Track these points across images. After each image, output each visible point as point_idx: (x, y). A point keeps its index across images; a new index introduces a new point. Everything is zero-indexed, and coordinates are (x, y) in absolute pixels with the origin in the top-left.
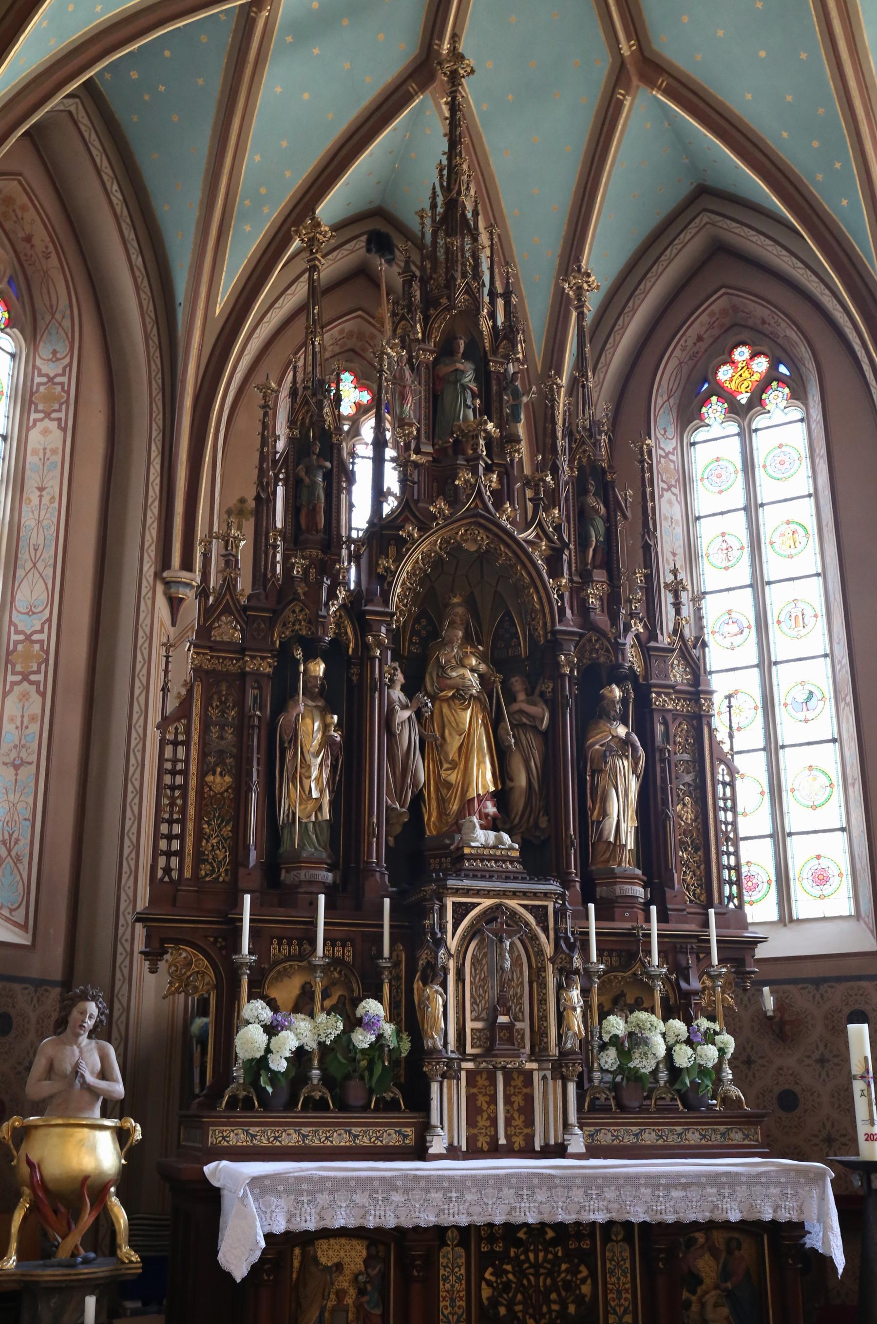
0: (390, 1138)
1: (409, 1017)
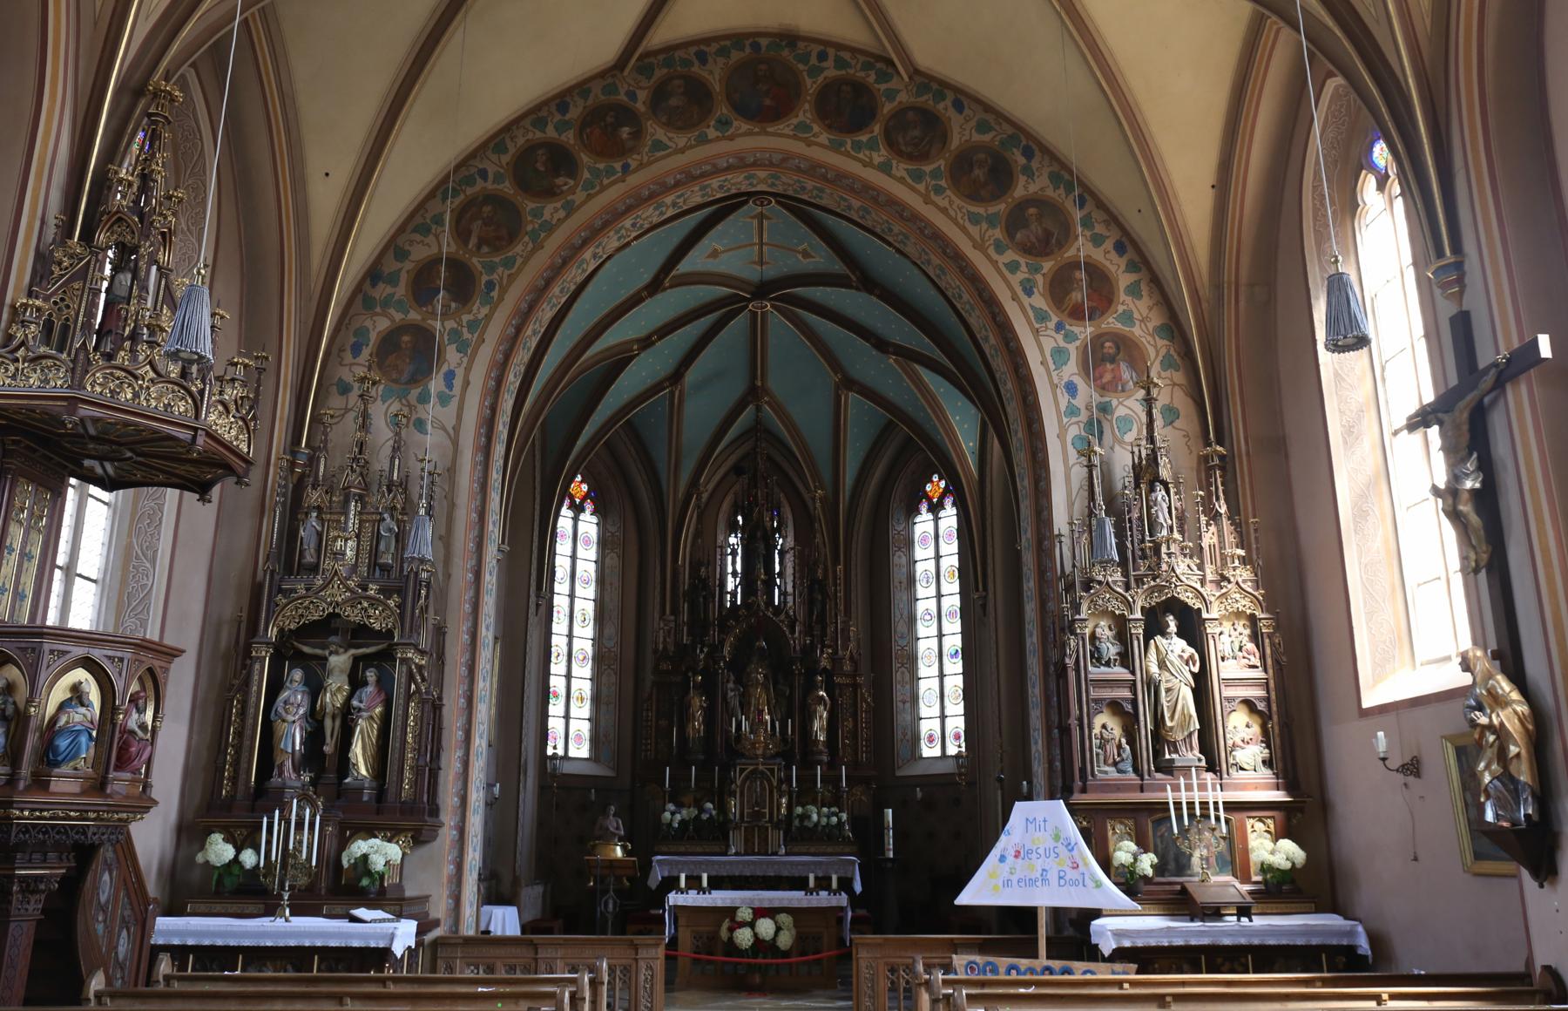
0: (717, 849)
1: (722, 807)
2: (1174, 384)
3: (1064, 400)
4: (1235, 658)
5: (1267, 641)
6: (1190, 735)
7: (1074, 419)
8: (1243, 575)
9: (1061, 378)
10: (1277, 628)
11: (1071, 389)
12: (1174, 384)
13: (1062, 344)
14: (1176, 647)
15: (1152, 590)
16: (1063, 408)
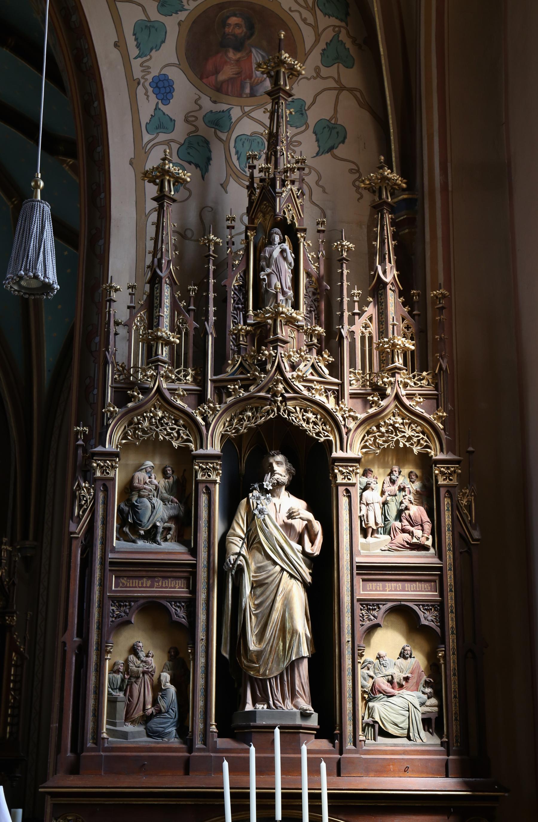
2: (342, 88)
3: (147, 106)
4: (387, 531)
5: (446, 502)
6: (292, 666)
7: (163, 137)
8: (408, 386)
9: (146, 70)
10: (465, 480)
11: (163, 88)
12: (342, 88)
13: (155, 15)
14: (281, 508)
15: (242, 405)
16: (145, 118)
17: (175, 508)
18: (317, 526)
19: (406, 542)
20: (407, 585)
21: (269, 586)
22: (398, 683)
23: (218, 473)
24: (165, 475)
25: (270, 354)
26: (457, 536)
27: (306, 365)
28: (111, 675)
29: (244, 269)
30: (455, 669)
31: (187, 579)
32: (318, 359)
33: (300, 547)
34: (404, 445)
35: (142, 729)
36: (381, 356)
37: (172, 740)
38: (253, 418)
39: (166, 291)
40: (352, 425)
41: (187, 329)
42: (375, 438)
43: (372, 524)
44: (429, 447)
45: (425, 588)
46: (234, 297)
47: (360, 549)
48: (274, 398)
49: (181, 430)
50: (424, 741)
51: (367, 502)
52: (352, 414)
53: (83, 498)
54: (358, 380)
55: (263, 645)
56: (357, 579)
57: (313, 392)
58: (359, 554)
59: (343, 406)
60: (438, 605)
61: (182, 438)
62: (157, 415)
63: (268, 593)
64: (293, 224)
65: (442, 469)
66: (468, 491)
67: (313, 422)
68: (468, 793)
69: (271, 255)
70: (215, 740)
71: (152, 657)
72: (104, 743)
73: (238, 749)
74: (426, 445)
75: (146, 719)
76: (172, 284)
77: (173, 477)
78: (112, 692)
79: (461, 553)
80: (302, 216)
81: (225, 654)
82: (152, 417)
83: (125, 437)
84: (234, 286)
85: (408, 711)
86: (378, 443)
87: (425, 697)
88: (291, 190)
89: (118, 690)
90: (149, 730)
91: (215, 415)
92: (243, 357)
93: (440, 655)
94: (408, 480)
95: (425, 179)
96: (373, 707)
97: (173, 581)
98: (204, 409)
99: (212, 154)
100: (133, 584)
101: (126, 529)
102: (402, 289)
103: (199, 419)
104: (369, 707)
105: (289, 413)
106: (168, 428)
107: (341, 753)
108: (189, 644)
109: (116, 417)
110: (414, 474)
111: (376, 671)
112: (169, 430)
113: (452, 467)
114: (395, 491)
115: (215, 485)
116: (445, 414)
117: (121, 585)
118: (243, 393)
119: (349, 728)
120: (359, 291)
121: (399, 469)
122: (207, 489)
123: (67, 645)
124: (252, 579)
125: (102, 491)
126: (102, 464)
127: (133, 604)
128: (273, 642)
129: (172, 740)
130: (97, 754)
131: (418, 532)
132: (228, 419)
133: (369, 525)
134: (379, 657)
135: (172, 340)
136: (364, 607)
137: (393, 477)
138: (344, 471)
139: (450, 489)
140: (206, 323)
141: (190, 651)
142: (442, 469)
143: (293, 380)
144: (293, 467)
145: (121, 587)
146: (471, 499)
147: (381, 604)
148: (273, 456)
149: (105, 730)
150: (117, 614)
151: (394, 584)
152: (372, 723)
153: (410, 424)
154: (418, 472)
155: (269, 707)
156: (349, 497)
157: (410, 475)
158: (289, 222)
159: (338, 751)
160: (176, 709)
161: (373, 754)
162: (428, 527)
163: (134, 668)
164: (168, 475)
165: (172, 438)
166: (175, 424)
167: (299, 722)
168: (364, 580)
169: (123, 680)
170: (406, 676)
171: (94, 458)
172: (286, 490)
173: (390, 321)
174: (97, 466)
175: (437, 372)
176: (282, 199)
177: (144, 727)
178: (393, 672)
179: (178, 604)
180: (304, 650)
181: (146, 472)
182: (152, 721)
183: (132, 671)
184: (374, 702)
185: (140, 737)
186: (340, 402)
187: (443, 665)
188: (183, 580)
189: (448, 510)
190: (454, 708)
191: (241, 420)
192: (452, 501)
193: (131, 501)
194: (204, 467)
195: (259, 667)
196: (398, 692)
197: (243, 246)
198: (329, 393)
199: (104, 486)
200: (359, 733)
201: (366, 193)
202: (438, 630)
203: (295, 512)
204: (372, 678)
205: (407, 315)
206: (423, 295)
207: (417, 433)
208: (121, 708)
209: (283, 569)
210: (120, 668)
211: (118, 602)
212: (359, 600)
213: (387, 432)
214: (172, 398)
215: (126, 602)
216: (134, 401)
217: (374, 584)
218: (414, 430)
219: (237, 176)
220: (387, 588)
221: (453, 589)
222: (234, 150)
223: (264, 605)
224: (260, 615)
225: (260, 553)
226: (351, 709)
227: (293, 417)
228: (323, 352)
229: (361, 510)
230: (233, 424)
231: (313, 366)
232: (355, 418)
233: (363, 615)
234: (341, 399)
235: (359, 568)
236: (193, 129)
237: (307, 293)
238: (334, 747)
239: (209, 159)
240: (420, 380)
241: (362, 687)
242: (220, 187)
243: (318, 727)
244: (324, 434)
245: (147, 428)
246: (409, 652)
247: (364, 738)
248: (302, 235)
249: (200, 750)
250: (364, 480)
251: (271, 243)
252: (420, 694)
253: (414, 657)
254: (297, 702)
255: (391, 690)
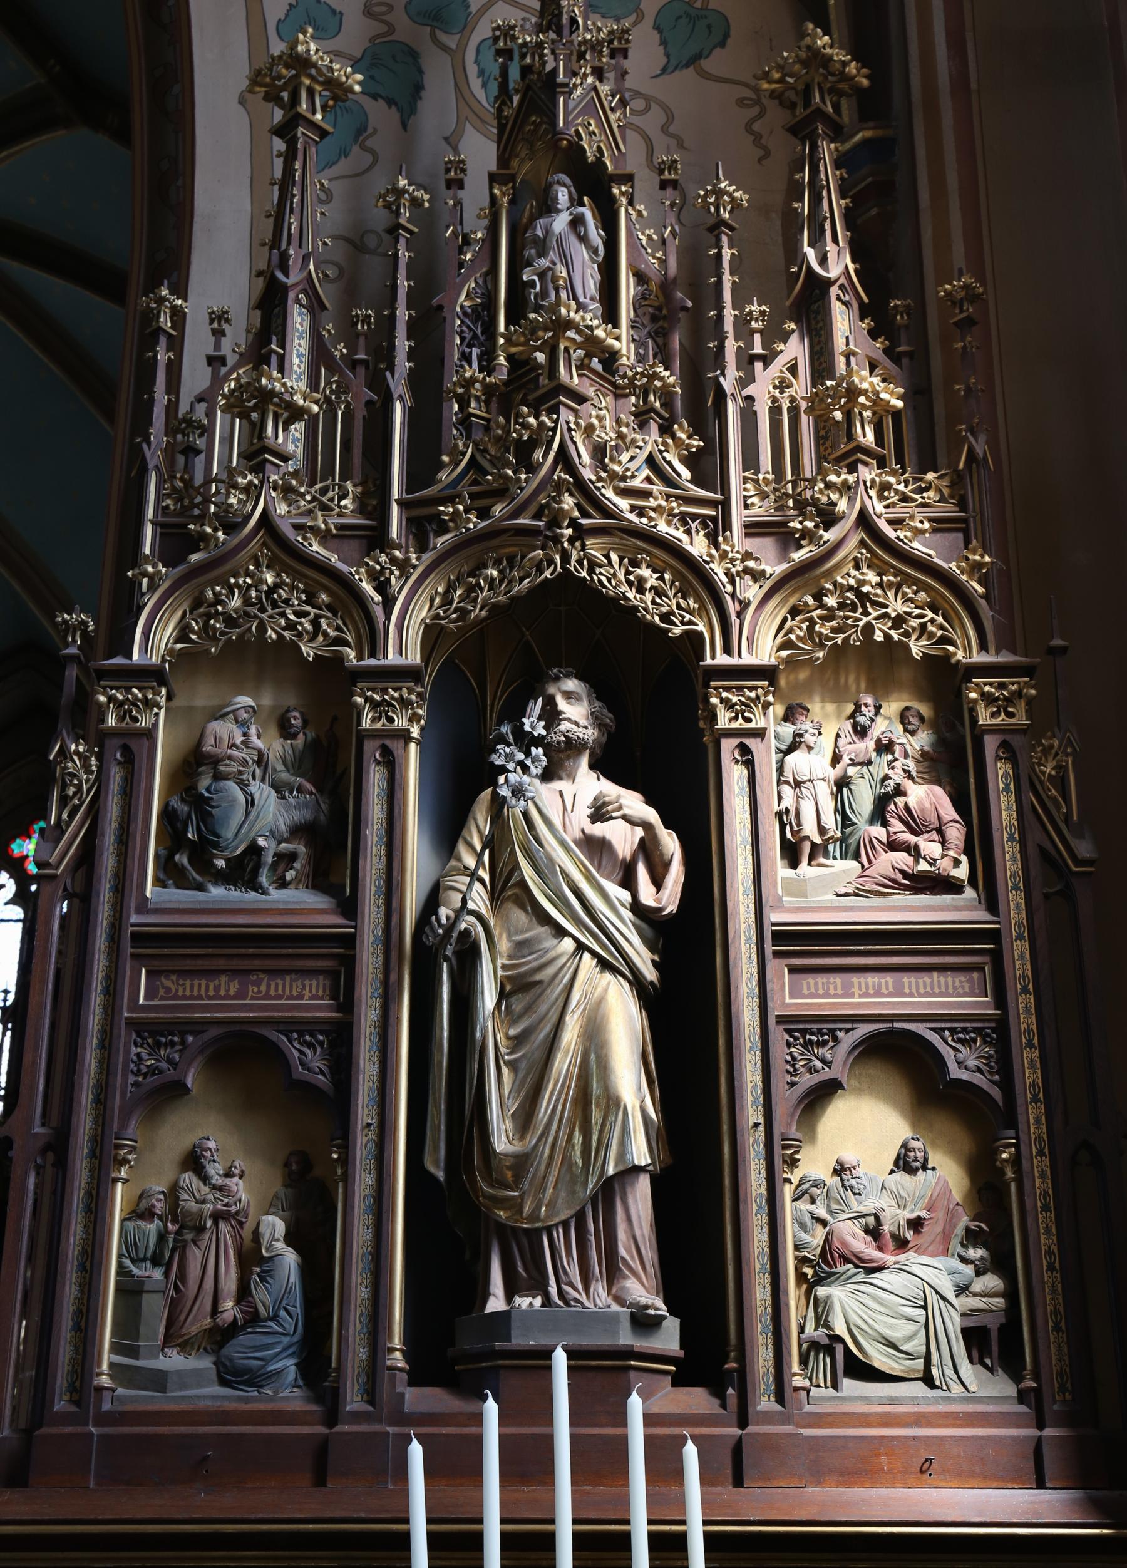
5: (999, 772)
6: (610, 1191)
14: (574, 806)
15: (473, 551)
17: (306, 805)
18: (670, 843)
19: (902, 872)
20: (907, 979)
21: (545, 990)
22: (893, 1235)
23: (415, 714)
24: (285, 730)
25: (541, 424)
26: (1032, 851)
27: (632, 458)
28: (130, 1225)
29: (484, 269)
30: (1046, 1193)
31: (333, 975)
32: (665, 444)
33: (626, 896)
34: (887, 636)
35: (205, 1363)
36: (822, 449)
37: (286, 1393)
38: (501, 581)
39: (299, 320)
40: (752, 591)
41: (348, 405)
42: (812, 622)
43: (810, 829)
44: (952, 643)
45: (955, 988)
46: (462, 331)
47: (780, 892)
48: (553, 532)
49: (322, 616)
50: (972, 1389)
51: (794, 779)
52: (751, 564)
53: (71, 781)
54: (764, 496)
55: (531, 1140)
56: (772, 965)
57: (652, 514)
58: (779, 906)
59: (728, 548)
60: (993, 1030)
61: (325, 634)
62: (262, 581)
63: (543, 1008)
64: (600, 162)
65: (987, 688)
66: (1056, 743)
67: (652, 588)
68: (1105, 1531)
69: (548, 231)
70: (399, 1389)
71: (241, 1177)
72: (99, 1401)
73: (461, 1414)
74: (942, 636)
75: (220, 1337)
76: (315, 307)
77: (305, 734)
78: (132, 1267)
79: (1047, 896)
80: (623, 150)
81: (432, 1169)
82: (249, 586)
83: (183, 634)
84: (462, 307)
85: (925, 1308)
86: (820, 634)
87: (969, 1270)
88: (595, 89)
89: (148, 1264)
90: (224, 1365)
91: (407, 578)
92: (476, 445)
93: (1004, 1156)
94: (901, 728)
95: (912, 76)
96: (828, 1297)
97: (295, 980)
98: (379, 563)
99: (425, 77)
100: (192, 990)
101: (182, 859)
102: (866, 300)
103: (367, 587)
104: (816, 1299)
105: (593, 566)
106: (288, 611)
107: (743, 1423)
108: (333, 1140)
109: (159, 586)
110: (912, 712)
111: (834, 1206)
112: (292, 617)
113: (1013, 684)
114: (867, 752)
115: (407, 744)
116: (987, 559)
117: (162, 992)
118: (474, 522)
119: (763, 1355)
120: (764, 307)
121: (876, 700)
122: (386, 752)
123: (15, 1146)
124: (500, 973)
125: (120, 763)
126: (121, 697)
127: (190, 1039)
128: (558, 1132)
129: (286, 1393)
130: (79, 1429)
131: (930, 847)
132: (440, 590)
133: (803, 834)
134: (840, 1170)
135: (301, 402)
136: (796, 1039)
137: (861, 719)
138: (735, 699)
139: (1008, 737)
140: (388, 374)
141: (335, 1156)
142: (987, 688)
143: (599, 485)
144: (609, 711)
145: (162, 998)
146: (1067, 762)
147: (840, 1030)
148: (557, 679)
149: (105, 1367)
150: (148, 1066)
151: (872, 979)
152: (826, 1341)
153: (899, 587)
154: (925, 709)
155: (547, 1302)
156: (750, 764)
157: (903, 717)
158: (590, 157)
159: (734, 1419)
160: (298, 1310)
161: (831, 1425)
162: (956, 834)
163: (192, 1206)
164: (292, 730)
165: (299, 635)
166: (307, 602)
167: (626, 1338)
168: (792, 970)
169: (162, 1237)
170: (914, 1215)
171: (102, 683)
172: (592, 767)
173: (840, 344)
174: (109, 701)
175: (961, 466)
176: (571, 104)
177: (212, 1358)
178: (878, 1205)
179: (308, 1038)
180: (638, 1148)
181: (237, 721)
182: (234, 1342)
183: (187, 1213)
184: (829, 1285)
185: (199, 1386)
186: (720, 539)
187: (1013, 1185)
188: (321, 978)
189: (1007, 789)
190: (1050, 1299)
191: (471, 589)
192: (1015, 767)
193: (195, 788)
194: (378, 698)
195: (522, 1197)
196: (893, 1258)
197: (486, 222)
198: (693, 525)
199: (126, 750)
200: (790, 1368)
201: (771, 105)
202: (996, 1093)
203: (610, 803)
204: (823, 1223)
205: (880, 356)
206: (918, 313)
207: (917, 607)
208: (155, 1309)
209: (581, 947)
210: (153, 1206)
211: (152, 1034)
212: (781, 1020)
213: (842, 606)
214: (299, 539)
215: (174, 1035)
216: (206, 548)
217: (821, 979)
218: (910, 600)
219: (482, 120)
220: (855, 990)
221: (1031, 987)
222: (475, 67)
223: (532, 1038)
224: (523, 1065)
225: (523, 907)
226: (769, 1303)
227: (602, 575)
228: (676, 426)
229: (780, 798)
230: (452, 600)
231: (650, 461)
232: (757, 576)
233: (794, 1059)
234: (724, 532)
235: (780, 937)
236: (385, 28)
237: (636, 315)
238: (724, 1406)
239: (418, 88)
240: (920, 490)
241: (797, 1247)
242: (443, 142)
243: (681, 1354)
244: (683, 617)
245: (236, 611)
246: (920, 1155)
247: (807, 1383)
248: (623, 189)
249: (357, 1417)
250: (788, 730)
251: (548, 207)
252: (956, 1263)
253: (933, 1169)
254: (623, 1288)
255: (876, 1254)
